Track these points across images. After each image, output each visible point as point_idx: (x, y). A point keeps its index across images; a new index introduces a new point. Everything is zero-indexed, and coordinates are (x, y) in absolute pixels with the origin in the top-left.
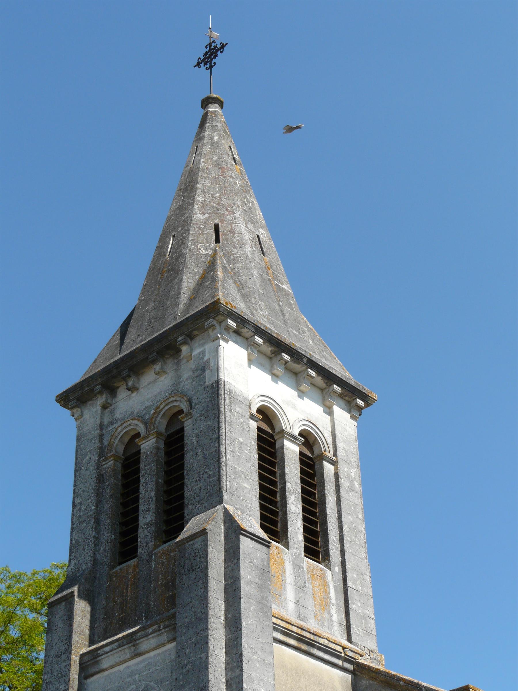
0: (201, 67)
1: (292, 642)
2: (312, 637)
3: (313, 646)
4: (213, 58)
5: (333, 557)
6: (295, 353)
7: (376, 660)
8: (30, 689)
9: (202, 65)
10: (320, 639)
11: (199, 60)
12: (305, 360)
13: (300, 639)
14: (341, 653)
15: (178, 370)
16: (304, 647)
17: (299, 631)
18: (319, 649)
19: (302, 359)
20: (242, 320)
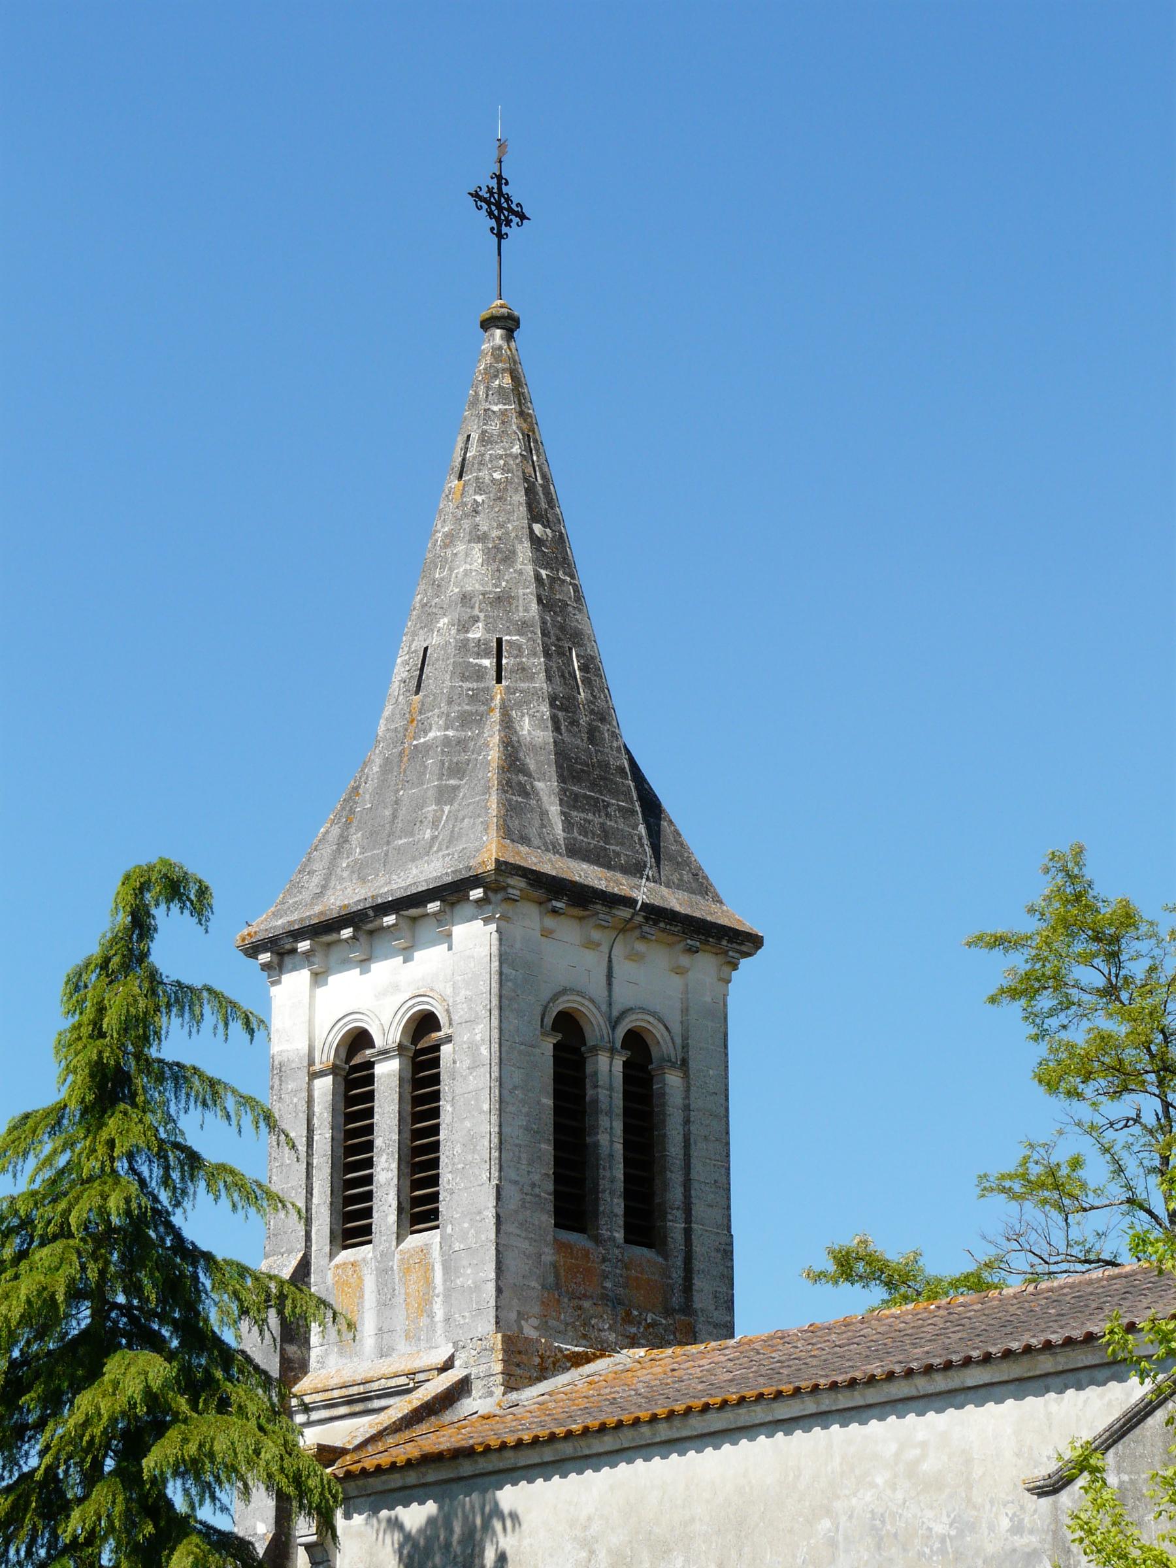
0: (506, 234)
1: (343, 1410)
2: (361, 1389)
3: (370, 1399)
4: (508, 204)
5: (444, 1213)
6: (353, 918)
7: (486, 1349)
8: (361, 1565)
9: (504, 229)
10: (372, 1384)
11: (495, 232)
12: (371, 913)
13: (350, 1401)
14: (408, 1384)
15: (604, 831)
16: (358, 1407)
17: (344, 1392)
18: (379, 1397)
19: (366, 915)
20: (271, 942)
